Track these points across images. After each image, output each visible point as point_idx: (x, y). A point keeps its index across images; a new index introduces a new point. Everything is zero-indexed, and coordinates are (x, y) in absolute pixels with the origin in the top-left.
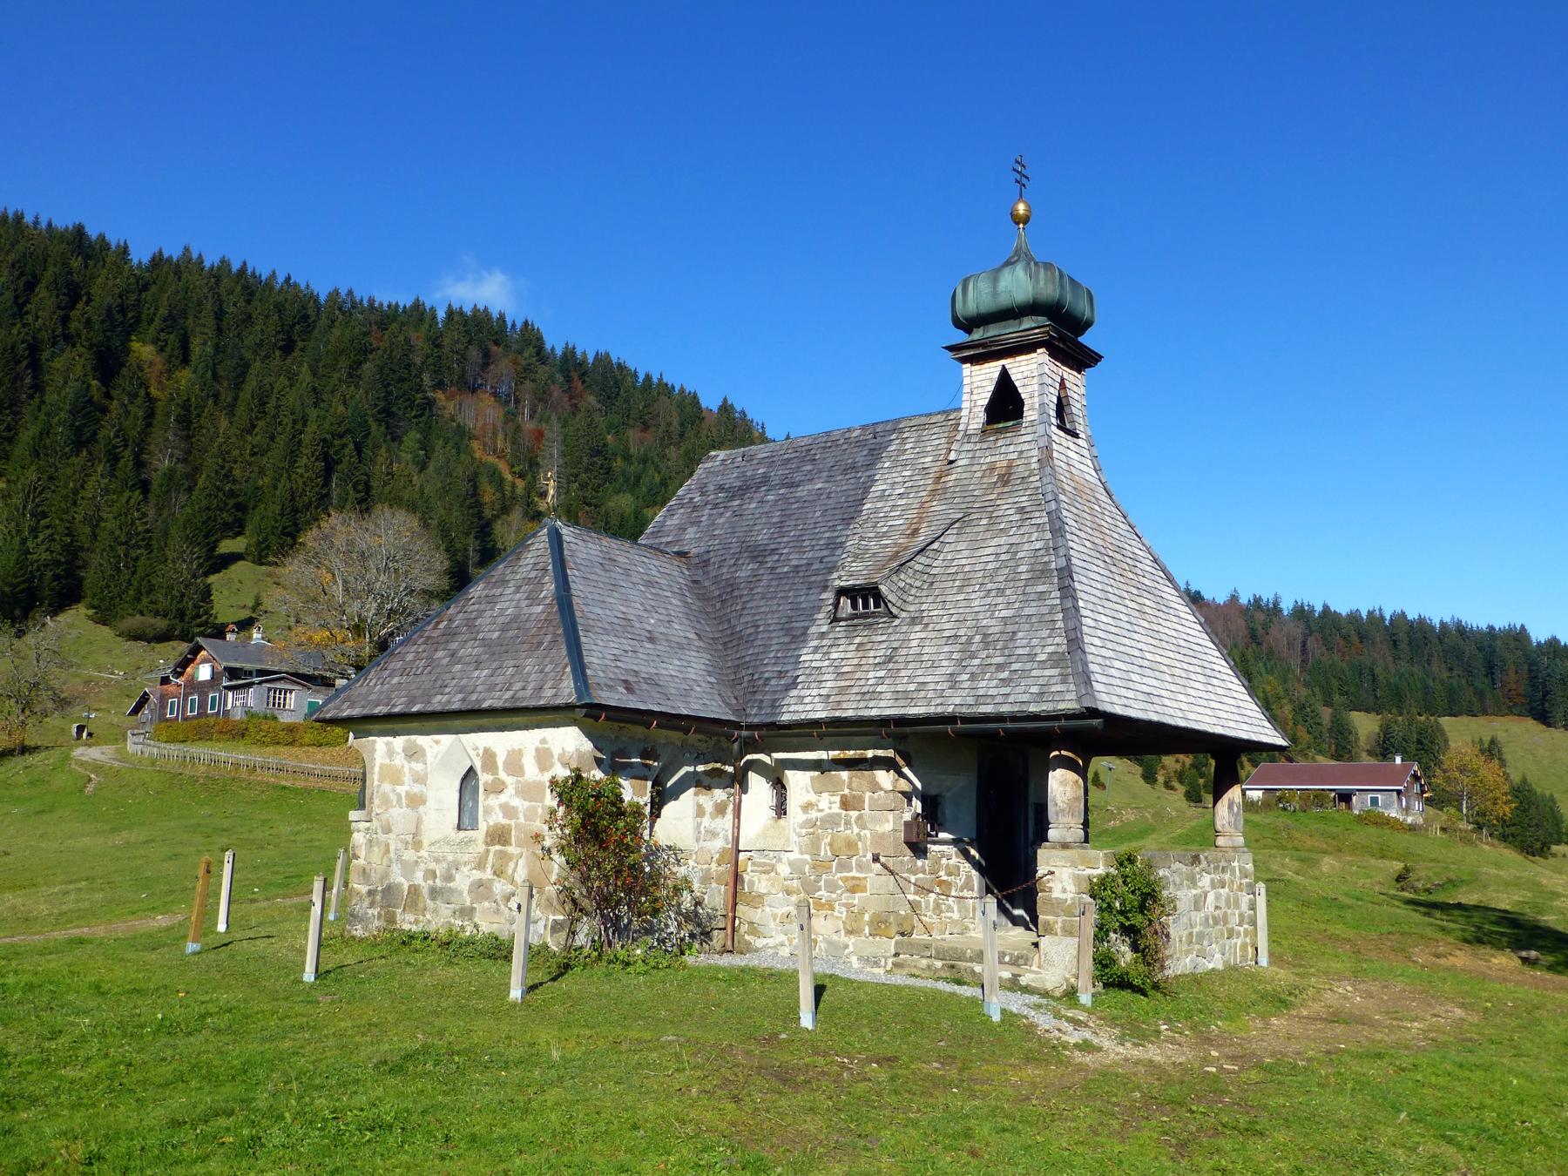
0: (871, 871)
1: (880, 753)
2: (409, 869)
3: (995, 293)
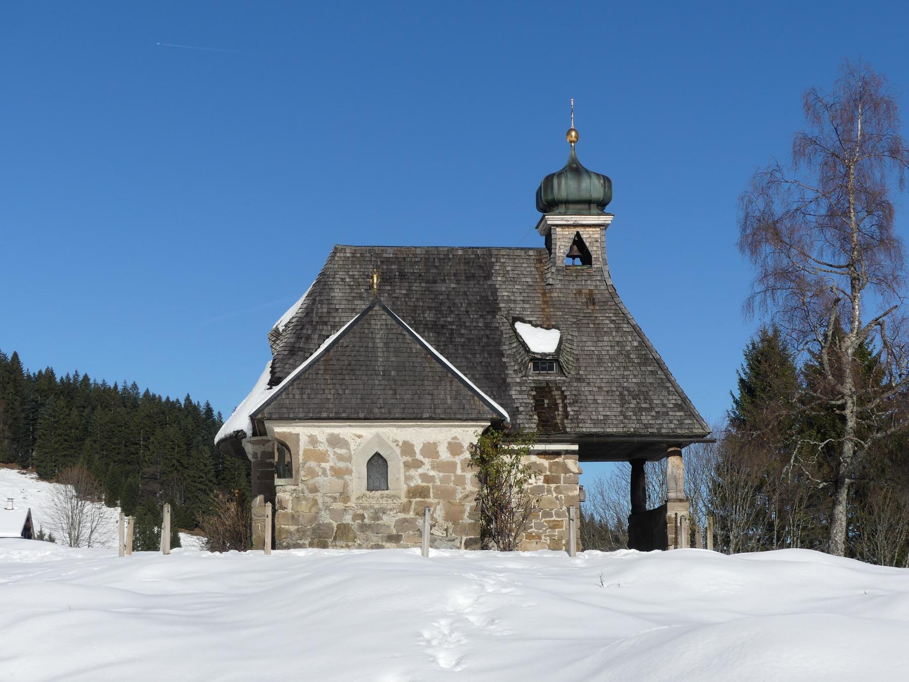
2: (334, 513)
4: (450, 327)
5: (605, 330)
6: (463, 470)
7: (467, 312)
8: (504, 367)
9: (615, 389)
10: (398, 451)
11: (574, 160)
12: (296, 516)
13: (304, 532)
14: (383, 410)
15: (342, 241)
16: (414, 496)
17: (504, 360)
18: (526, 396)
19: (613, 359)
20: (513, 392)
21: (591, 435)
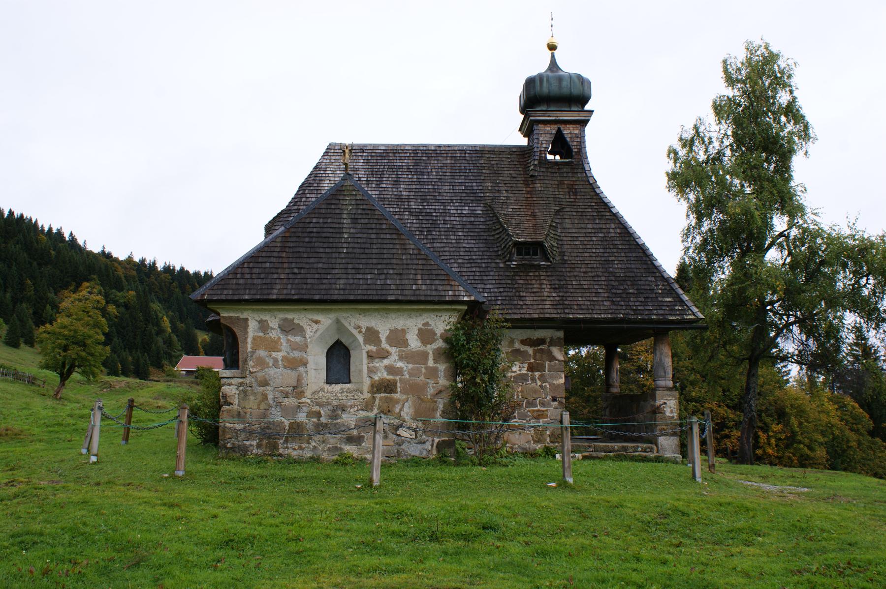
0: (551, 406)
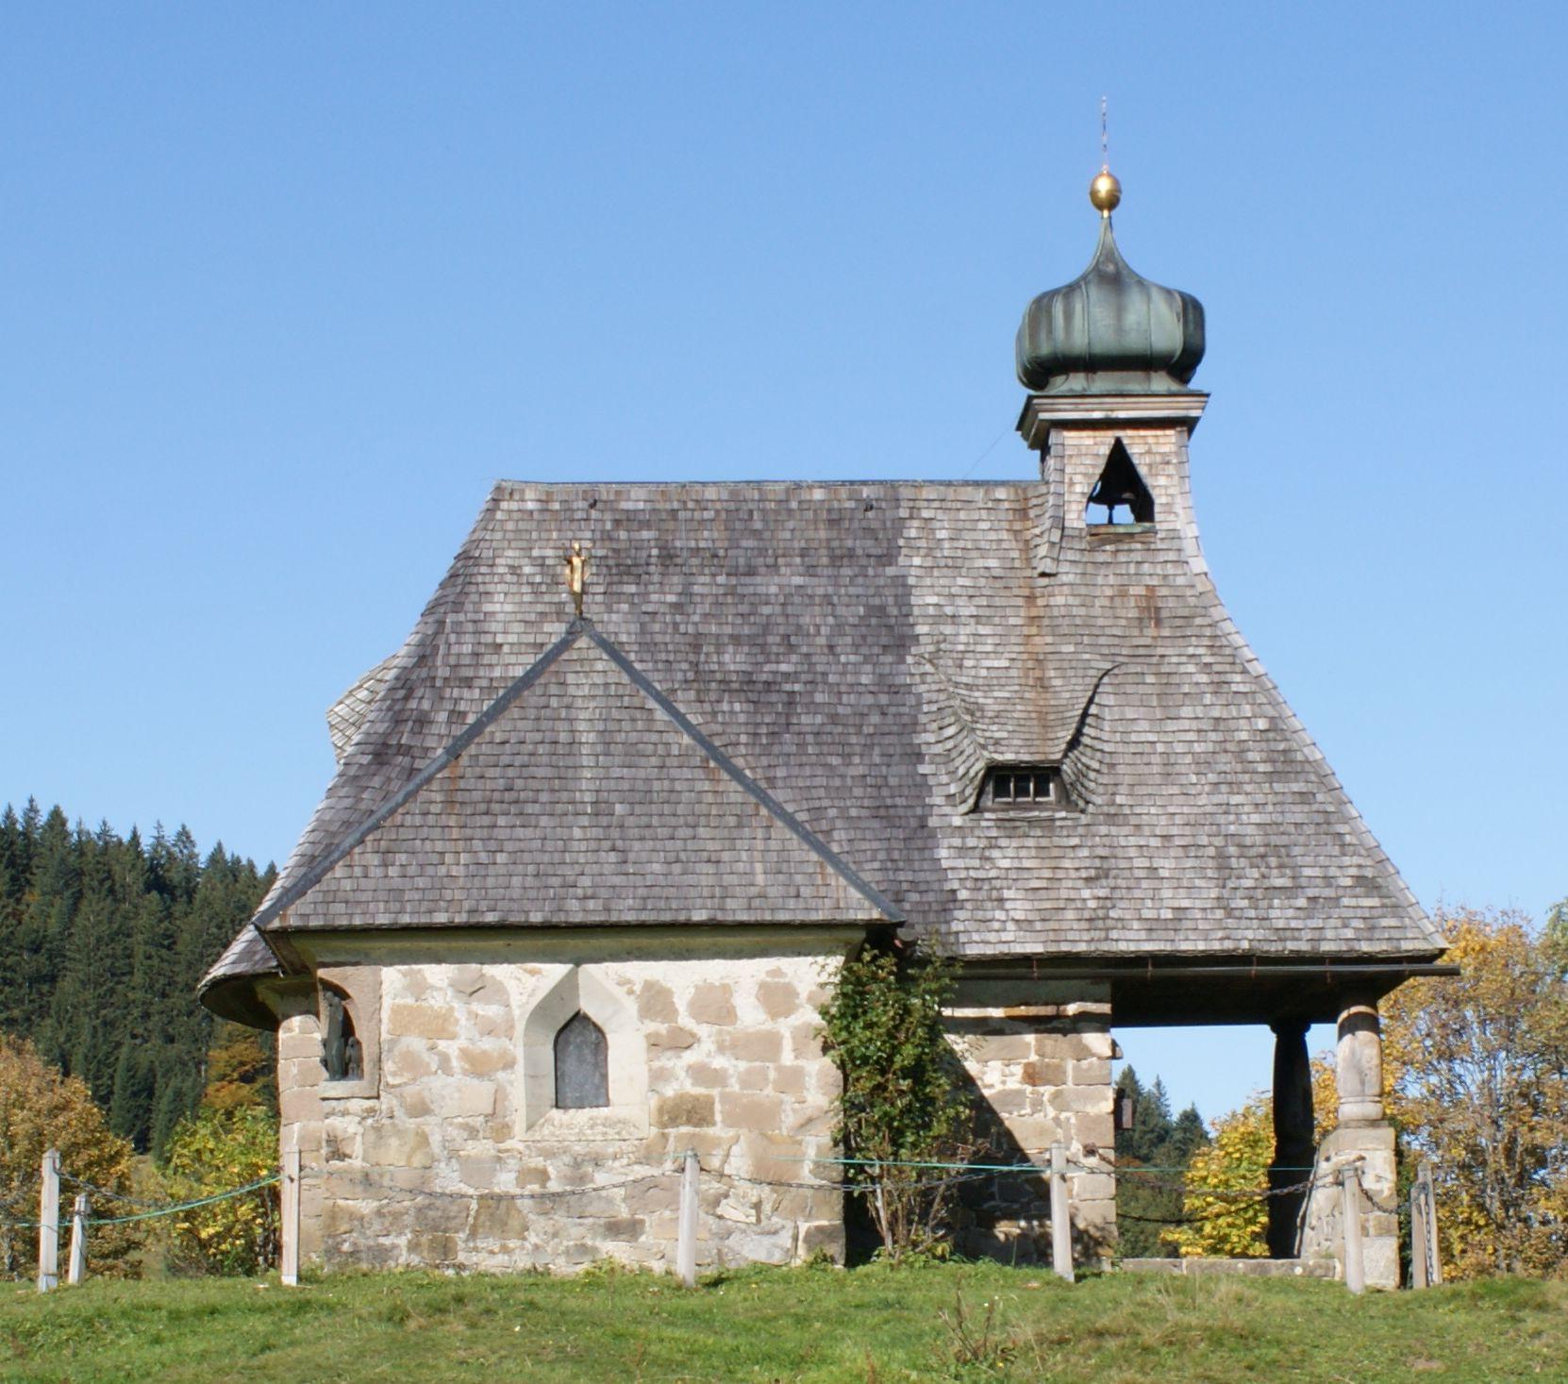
1: (1092, 1007)
2: (471, 1169)
3: (1120, 329)
4: (787, 687)
5: (1186, 689)
6: (798, 1053)
7: (831, 647)
8: (923, 786)
9: (1205, 841)
10: (631, 1006)
11: (1109, 254)
12: (374, 1177)
13: (397, 1216)
14: (591, 904)
15: (512, 472)
16: (674, 1121)
17: (923, 769)
18: (976, 863)
19: (1202, 764)
20: (943, 853)
21: (1139, 960)
